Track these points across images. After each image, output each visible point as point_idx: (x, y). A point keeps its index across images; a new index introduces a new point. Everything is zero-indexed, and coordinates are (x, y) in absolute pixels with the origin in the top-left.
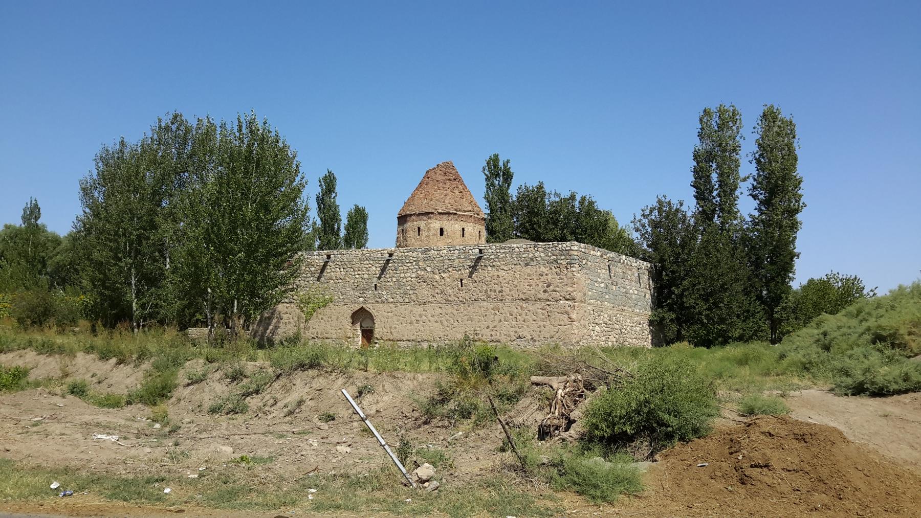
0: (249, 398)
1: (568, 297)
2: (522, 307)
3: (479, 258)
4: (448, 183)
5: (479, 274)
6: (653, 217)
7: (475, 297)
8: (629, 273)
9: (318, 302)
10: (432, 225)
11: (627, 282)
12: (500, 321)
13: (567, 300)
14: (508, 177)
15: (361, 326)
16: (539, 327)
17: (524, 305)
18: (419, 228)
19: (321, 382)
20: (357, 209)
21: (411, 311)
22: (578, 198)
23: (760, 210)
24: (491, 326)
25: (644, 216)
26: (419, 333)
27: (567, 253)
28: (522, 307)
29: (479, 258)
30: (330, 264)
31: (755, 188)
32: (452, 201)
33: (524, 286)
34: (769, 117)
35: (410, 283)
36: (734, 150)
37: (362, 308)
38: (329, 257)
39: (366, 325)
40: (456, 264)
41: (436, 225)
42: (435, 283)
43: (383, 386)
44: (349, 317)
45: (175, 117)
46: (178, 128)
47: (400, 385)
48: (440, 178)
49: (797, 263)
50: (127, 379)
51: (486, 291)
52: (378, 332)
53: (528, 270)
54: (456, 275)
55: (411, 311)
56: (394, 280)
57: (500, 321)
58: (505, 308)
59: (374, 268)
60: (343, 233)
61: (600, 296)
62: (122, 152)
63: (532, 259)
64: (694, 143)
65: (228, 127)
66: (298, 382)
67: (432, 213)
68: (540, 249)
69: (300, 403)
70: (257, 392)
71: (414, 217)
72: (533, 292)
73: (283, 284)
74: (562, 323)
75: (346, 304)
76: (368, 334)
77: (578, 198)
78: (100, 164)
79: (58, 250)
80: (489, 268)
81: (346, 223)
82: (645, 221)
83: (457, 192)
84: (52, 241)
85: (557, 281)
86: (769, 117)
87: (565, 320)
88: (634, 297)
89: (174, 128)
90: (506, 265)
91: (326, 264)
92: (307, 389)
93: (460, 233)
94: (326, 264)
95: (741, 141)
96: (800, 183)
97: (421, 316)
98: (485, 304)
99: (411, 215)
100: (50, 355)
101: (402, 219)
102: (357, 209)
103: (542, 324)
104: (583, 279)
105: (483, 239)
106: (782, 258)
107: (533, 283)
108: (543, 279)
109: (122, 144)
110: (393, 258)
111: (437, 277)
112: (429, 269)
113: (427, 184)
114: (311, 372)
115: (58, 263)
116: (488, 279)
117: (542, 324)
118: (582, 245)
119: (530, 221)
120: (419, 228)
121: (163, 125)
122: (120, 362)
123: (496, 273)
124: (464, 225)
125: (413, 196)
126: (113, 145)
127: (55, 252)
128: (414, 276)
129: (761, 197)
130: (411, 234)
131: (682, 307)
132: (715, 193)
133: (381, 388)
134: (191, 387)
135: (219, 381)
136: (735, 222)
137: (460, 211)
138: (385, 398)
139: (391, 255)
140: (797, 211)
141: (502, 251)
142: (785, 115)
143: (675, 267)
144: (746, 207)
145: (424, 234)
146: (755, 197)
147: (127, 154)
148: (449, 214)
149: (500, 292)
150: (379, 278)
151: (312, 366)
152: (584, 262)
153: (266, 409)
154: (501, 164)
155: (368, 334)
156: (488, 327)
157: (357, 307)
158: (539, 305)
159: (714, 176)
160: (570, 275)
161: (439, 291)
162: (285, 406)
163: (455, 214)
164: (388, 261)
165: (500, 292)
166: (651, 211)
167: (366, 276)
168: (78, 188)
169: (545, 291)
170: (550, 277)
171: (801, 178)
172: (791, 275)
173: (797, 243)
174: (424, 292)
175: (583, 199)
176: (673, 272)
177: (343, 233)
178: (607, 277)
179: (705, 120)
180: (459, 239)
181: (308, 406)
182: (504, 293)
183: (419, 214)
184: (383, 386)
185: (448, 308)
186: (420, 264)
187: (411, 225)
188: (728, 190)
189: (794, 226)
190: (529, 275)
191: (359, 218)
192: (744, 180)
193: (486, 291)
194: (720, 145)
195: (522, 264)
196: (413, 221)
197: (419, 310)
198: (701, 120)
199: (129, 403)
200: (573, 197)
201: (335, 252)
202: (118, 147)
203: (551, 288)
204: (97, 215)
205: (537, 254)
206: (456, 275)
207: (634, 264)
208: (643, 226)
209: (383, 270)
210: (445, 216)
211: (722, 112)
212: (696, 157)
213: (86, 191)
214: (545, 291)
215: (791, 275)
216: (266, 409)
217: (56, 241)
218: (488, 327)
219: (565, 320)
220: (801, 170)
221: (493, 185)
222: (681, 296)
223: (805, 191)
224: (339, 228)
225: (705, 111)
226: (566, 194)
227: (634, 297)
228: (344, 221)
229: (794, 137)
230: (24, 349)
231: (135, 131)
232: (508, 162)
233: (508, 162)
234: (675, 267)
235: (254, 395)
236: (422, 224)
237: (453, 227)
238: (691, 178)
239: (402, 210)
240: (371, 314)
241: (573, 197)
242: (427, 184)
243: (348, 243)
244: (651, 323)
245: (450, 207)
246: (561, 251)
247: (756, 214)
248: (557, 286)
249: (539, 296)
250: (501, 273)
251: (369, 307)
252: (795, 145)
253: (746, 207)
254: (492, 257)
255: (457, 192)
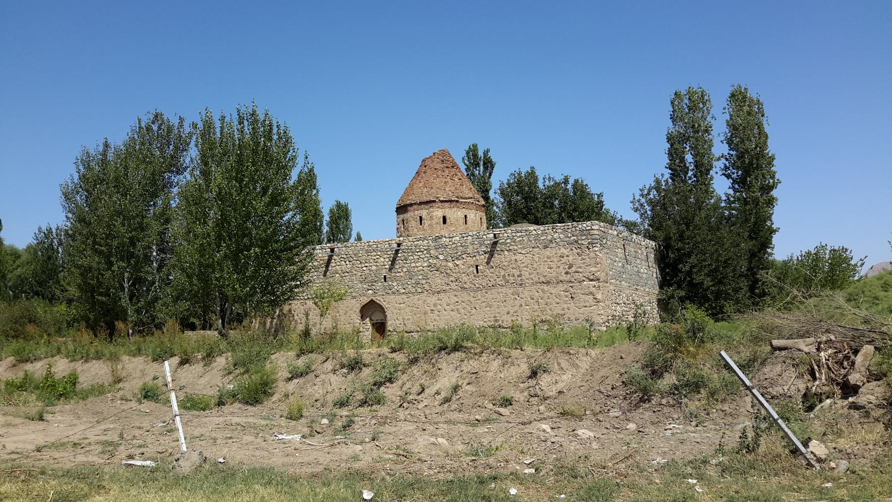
0: (382, 389)
1: (592, 277)
2: (543, 290)
3: (495, 243)
4: (447, 171)
5: (497, 258)
6: (652, 196)
7: (493, 282)
8: (640, 251)
9: (327, 297)
10: (434, 214)
11: (638, 261)
12: (521, 305)
13: (591, 280)
14: (489, 165)
15: (371, 319)
16: (563, 309)
17: (545, 287)
18: (421, 218)
19: (473, 365)
20: (339, 205)
21: (425, 301)
22: (571, 181)
23: (735, 190)
24: (512, 312)
25: (642, 195)
26: (435, 323)
27: (587, 233)
28: (543, 290)
29: (495, 243)
30: (335, 257)
31: (726, 168)
32: (453, 189)
33: (544, 269)
34: (738, 98)
35: (421, 272)
36: (707, 131)
37: (372, 301)
38: (332, 250)
39: (377, 317)
40: (469, 250)
41: (438, 213)
42: (448, 271)
43: (559, 364)
44: (358, 311)
45: (156, 116)
46: (159, 128)
47: (577, 362)
48: (439, 166)
49: (776, 239)
50: (210, 378)
51: (504, 276)
52: (390, 325)
53: (548, 252)
54: (471, 261)
55: (425, 301)
56: (405, 270)
57: (521, 305)
58: (526, 293)
59: (382, 259)
60: (325, 229)
61: (619, 276)
62: (104, 154)
63: (551, 241)
64: (667, 126)
65: (227, 119)
66: (444, 365)
67: (434, 201)
68: (560, 231)
69: (456, 388)
70: (390, 380)
71: (415, 207)
72: (554, 274)
73: (293, 279)
74: (587, 304)
75: (354, 297)
76: (380, 328)
77: (571, 181)
78: (81, 167)
79: (18, 263)
80: (506, 253)
81: (328, 219)
82: (643, 200)
83: (456, 179)
84: (11, 255)
85: (579, 261)
86: (738, 98)
87: (590, 301)
88: (644, 276)
89: (155, 127)
90: (524, 248)
91: (330, 258)
92: (457, 373)
93: (462, 221)
94: (330, 258)
95: (713, 121)
96: (773, 159)
97: (435, 305)
98: (504, 290)
99: (411, 205)
100: (86, 361)
101: (402, 209)
102: (339, 205)
103: (565, 306)
104: (604, 258)
105: (485, 225)
106: (761, 235)
107: (553, 265)
108: (564, 260)
109: (106, 145)
110: (402, 247)
111: (450, 264)
112: (441, 257)
113: (425, 173)
114: (458, 355)
115: (19, 276)
116: (506, 264)
117: (565, 306)
118: (602, 224)
119: (527, 207)
120: (421, 218)
121: (143, 125)
122: (184, 362)
123: (513, 258)
124: (466, 212)
125: (411, 186)
126: (95, 148)
127: (14, 266)
128: (426, 264)
129: (735, 176)
130: (413, 224)
131: (691, 284)
132: (690, 173)
133: (557, 367)
134: (296, 381)
135: (334, 371)
136: (712, 201)
137: (462, 198)
138: (564, 377)
139: (399, 245)
140: (771, 188)
141: (518, 234)
142: (752, 94)
143: (680, 245)
144: (721, 186)
145: (426, 223)
146: (728, 176)
147: (110, 156)
148: (451, 201)
149: (518, 276)
150: (390, 269)
151: (457, 348)
152: (604, 241)
153: (411, 397)
154: (481, 154)
155: (380, 328)
156: (508, 313)
157: (365, 300)
158: (561, 287)
159: (689, 158)
160: (592, 255)
161: (453, 279)
162: (438, 393)
163: (457, 201)
164: (397, 251)
165: (518, 276)
166: (649, 190)
167: (374, 268)
168: (60, 194)
169: (567, 273)
170: (571, 258)
171: (773, 156)
172: (769, 250)
173: (773, 218)
174: (438, 281)
175: (576, 181)
176: (678, 250)
177: (325, 229)
178: (623, 256)
179: (676, 103)
180: (462, 227)
181: (466, 392)
182: (523, 277)
183: (421, 203)
184: (559, 364)
185: (465, 296)
186: (432, 252)
187: (412, 215)
188: (703, 169)
189: (771, 202)
190: (549, 257)
191: (341, 215)
192: (719, 159)
193: (504, 276)
194: (693, 126)
195: (535, 249)
196: (414, 210)
197: (433, 299)
198: (672, 103)
199: (221, 403)
200: (566, 181)
201: (339, 245)
202: (101, 149)
203: (574, 269)
204: (81, 220)
205: (556, 236)
206: (471, 261)
207: (643, 243)
208: (642, 205)
209: (393, 262)
210: (447, 204)
211: (690, 93)
212: (670, 139)
213: (67, 197)
214: (567, 273)
215: (769, 250)
216: (411, 397)
217: (15, 254)
218: (508, 313)
219: (590, 301)
220: (772, 148)
221: (473, 175)
222: (689, 273)
223: (778, 167)
224: (321, 224)
225: (676, 94)
226: (559, 178)
227: (644, 276)
228: (326, 218)
229: (763, 116)
230: (52, 356)
231: (113, 129)
232: (488, 151)
233: (488, 151)
234: (680, 245)
235: (388, 384)
236: (424, 213)
237: (455, 214)
238: (666, 160)
239: (401, 199)
240: (383, 308)
241: (566, 181)
242: (425, 173)
243: (333, 237)
244: (659, 301)
245: (451, 194)
246: (582, 231)
247: (731, 192)
248: (580, 267)
249: (561, 278)
250: (519, 257)
251: (379, 299)
252: (765, 123)
253: (721, 186)
254: (509, 241)
255: (456, 179)
